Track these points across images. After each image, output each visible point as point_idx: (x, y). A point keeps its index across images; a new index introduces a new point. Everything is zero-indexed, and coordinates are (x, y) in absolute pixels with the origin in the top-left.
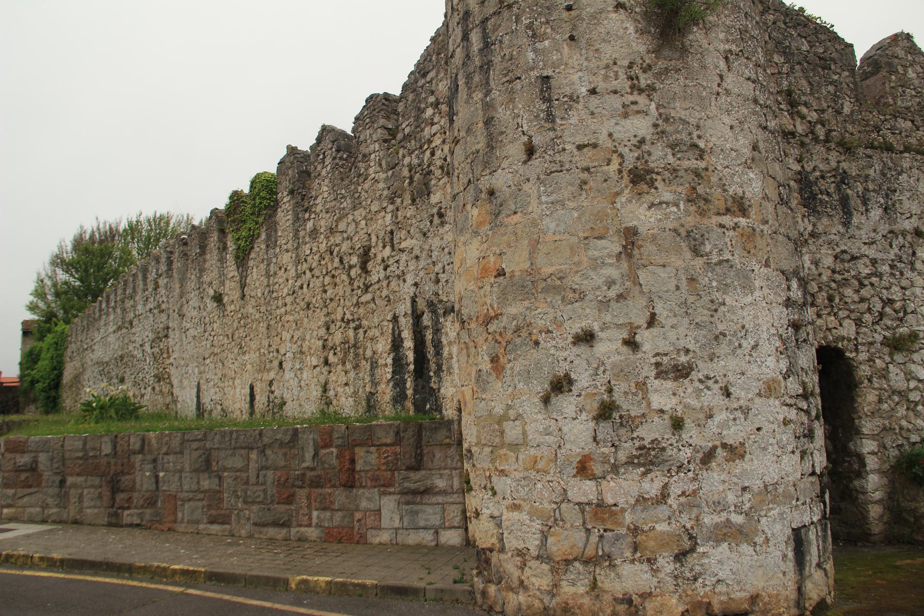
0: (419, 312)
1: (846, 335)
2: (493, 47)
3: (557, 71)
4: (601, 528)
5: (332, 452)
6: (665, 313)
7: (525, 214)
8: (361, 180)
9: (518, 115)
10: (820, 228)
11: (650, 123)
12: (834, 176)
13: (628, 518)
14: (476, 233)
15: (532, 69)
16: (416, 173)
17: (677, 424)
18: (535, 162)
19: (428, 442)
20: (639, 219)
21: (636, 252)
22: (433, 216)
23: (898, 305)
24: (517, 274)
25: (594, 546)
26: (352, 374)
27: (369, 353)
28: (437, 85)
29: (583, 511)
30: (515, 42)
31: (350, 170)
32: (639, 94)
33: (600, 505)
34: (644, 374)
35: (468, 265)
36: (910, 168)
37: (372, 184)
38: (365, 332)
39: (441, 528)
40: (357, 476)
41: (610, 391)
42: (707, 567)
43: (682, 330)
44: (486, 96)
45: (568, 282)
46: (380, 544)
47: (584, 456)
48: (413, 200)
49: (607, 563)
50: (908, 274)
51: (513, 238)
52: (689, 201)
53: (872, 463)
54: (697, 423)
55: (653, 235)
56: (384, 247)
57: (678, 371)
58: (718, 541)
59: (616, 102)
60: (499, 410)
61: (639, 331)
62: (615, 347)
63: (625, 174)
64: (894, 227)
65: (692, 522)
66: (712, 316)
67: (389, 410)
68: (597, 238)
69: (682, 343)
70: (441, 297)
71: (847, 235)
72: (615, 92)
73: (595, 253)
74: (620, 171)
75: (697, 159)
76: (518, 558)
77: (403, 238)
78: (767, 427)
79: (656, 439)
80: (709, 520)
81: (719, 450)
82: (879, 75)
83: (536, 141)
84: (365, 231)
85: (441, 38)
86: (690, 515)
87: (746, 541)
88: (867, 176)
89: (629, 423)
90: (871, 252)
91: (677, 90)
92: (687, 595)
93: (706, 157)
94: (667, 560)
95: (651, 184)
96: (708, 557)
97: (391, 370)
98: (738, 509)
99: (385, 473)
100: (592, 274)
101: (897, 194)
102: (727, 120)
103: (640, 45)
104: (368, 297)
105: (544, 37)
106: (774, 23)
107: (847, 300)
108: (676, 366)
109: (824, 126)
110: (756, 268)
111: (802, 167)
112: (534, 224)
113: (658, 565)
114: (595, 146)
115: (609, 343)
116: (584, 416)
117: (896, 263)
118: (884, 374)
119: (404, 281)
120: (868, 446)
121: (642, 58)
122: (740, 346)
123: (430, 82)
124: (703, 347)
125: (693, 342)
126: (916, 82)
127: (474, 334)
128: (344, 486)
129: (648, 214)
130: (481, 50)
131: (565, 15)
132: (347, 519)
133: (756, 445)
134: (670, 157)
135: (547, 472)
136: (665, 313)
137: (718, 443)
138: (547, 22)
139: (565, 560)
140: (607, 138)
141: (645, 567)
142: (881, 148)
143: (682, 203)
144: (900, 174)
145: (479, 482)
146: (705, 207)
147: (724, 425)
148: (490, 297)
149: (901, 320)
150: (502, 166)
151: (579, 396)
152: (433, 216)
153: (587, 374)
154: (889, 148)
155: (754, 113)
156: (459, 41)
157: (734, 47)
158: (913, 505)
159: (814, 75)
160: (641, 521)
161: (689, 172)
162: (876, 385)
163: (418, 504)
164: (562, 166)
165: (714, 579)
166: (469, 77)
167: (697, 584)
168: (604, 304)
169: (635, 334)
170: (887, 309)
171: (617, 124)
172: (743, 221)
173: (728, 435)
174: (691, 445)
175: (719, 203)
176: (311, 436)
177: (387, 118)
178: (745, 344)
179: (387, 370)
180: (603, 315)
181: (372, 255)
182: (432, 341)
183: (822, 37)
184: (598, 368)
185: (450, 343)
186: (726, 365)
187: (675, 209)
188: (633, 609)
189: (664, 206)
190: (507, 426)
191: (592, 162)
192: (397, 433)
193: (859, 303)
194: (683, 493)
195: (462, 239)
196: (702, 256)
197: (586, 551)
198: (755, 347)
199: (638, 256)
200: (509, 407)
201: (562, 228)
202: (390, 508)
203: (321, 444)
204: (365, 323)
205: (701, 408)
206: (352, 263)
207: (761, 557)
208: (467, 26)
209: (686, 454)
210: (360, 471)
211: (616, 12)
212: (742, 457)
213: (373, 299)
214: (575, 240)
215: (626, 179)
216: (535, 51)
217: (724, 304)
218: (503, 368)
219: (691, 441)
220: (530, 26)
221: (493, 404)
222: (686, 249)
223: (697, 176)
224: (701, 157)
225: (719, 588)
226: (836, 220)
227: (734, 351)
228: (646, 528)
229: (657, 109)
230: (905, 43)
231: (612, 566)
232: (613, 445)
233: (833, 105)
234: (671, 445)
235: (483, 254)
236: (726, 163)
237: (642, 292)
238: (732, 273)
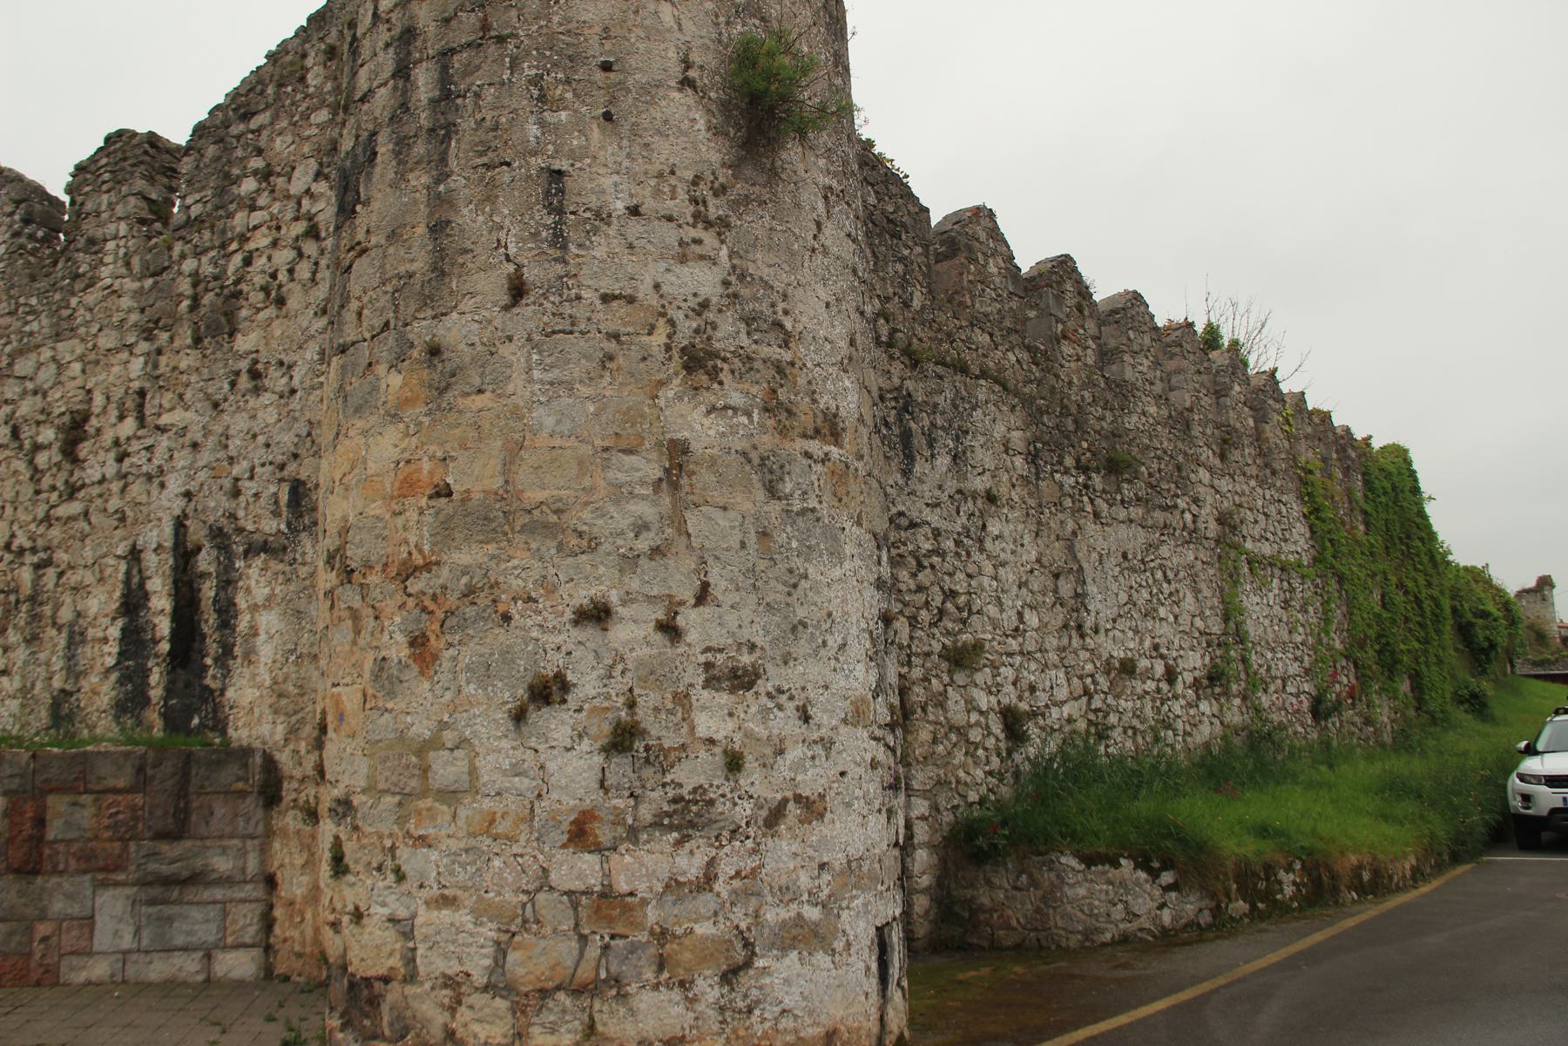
0: (190, 546)
2: (459, 101)
3: (578, 165)
4: (606, 933)
6: (723, 584)
7: (500, 396)
8: (78, 285)
9: (498, 228)
11: (719, 278)
12: (895, 399)
13: (652, 915)
14: (394, 417)
15: (534, 154)
16: (207, 290)
17: (734, 763)
18: (526, 310)
19: (202, 787)
20: (692, 429)
21: (684, 481)
22: (238, 373)
23: (962, 600)
24: (476, 496)
25: (593, 964)
26: (21, 654)
27: (66, 615)
28: (272, 140)
29: (575, 906)
30: (506, 102)
31: (55, 263)
32: (706, 229)
33: (607, 894)
34: (687, 680)
35: (369, 472)
37: (105, 298)
38: (61, 574)
39: (216, 947)
40: (47, 851)
41: (631, 705)
42: (768, 990)
43: (746, 613)
44: (438, 182)
45: (571, 519)
46: (89, 983)
47: (584, 813)
48: (197, 341)
49: (614, 992)
50: (976, 556)
51: (472, 434)
52: (767, 410)
55: (711, 457)
56: (121, 418)
57: (736, 677)
58: (784, 950)
60: (421, 729)
61: (681, 609)
62: (643, 634)
63: (675, 353)
65: (749, 920)
66: (789, 594)
67: (105, 725)
68: (623, 451)
69: (745, 634)
70: (242, 523)
71: (907, 490)
72: (670, 219)
73: (619, 475)
74: (668, 348)
76: (444, 992)
77: (167, 405)
78: (854, 772)
80: (774, 915)
81: (791, 805)
82: (956, 261)
83: (530, 274)
84: (79, 382)
85: (289, 58)
88: (936, 405)
89: (660, 759)
90: (934, 518)
91: (760, 233)
94: (710, 981)
95: (714, 374)
96: (770, 975)
97: (115, 650)
99: (108, 845)
104: (75, 507)
105: (559, 105)
108: (734, 670)
109: (887, 321)
110: (848, 525)
112: (516, 414)
113: (696, 990)
114: (631, 300)
115: (633, 626)
116: (586, 745)
118: (941, 702)
119: (162, 486)
122: (824, 643)
123: (258, 131)
124: (774, 642)
126: (997, 280)
127: (376, 593)
128: (17, 871)
129: (707, 422)
130: (433, 102)
131: (599, 76)
132: (17, 938)
134: (743, 336)
135: (512, 839)
136: (723, 584)
137: (789, 794)
138: (568, 82)
139: (540, 990)
140: (651, 291)
141: (676, 995)
142: (955, 367)
144: (974, 409)
145: (365, 859)
147: (799, 766)
148: (416, 529)
149: (964, 622)
150: (462, 307)
151: (579, 710)
152: (238, 373)
153: (595, 674)
154: (963, 369)
155: (853, 289)
156: (386, 74)
157: (834, 184)
158: (969, 893)
160: (671, 920)
162: (932, 718)
163: (173, 903)
164: (573, 324)
165: (777, 1009)
166: (402, 144)
168: (629, 561)
169: (676, 613)
171: (668, 270)
172: (835, 452)
175: (806, 420)
177: (151, 180)
179: (106, 649)
181: (92, 431)
182: (215, 601)
183: (894, 190)
185: (254, 608)
186: (805, 673)
187: (744, 420)
189: (730, 412)
190: (438, 759)
191: (625, 325)
192: (140, 769)
194: (738, 873)
195: (360, 424)
197: (579, 972)
198: (843, 647)
199: (687, 489)
200: (443, 726)
201: (566, 427)
202: (114, 915)
204: (61, 556)
206: (40, 439)
208: (409, 53)
209: (745, 809)
210: (55, 842)
211: (680, 90)
212: (821, 816)
213: (86, 514)
214: (587, 450)
216: (542, 124)
217: (806, 577)
218: (435, 657)
219: (752, 791)
220: (536, 81)
221: (409, 719)
222: (759, 485)
224: (786, 345)
227: (816, 652)
228: (679, 931)
230: (985, 222)
231: (622, 997)
232: (632, 795)
234: (723, 796)
235: (406, 455)
236: (817, 359)
237: (689, 547)
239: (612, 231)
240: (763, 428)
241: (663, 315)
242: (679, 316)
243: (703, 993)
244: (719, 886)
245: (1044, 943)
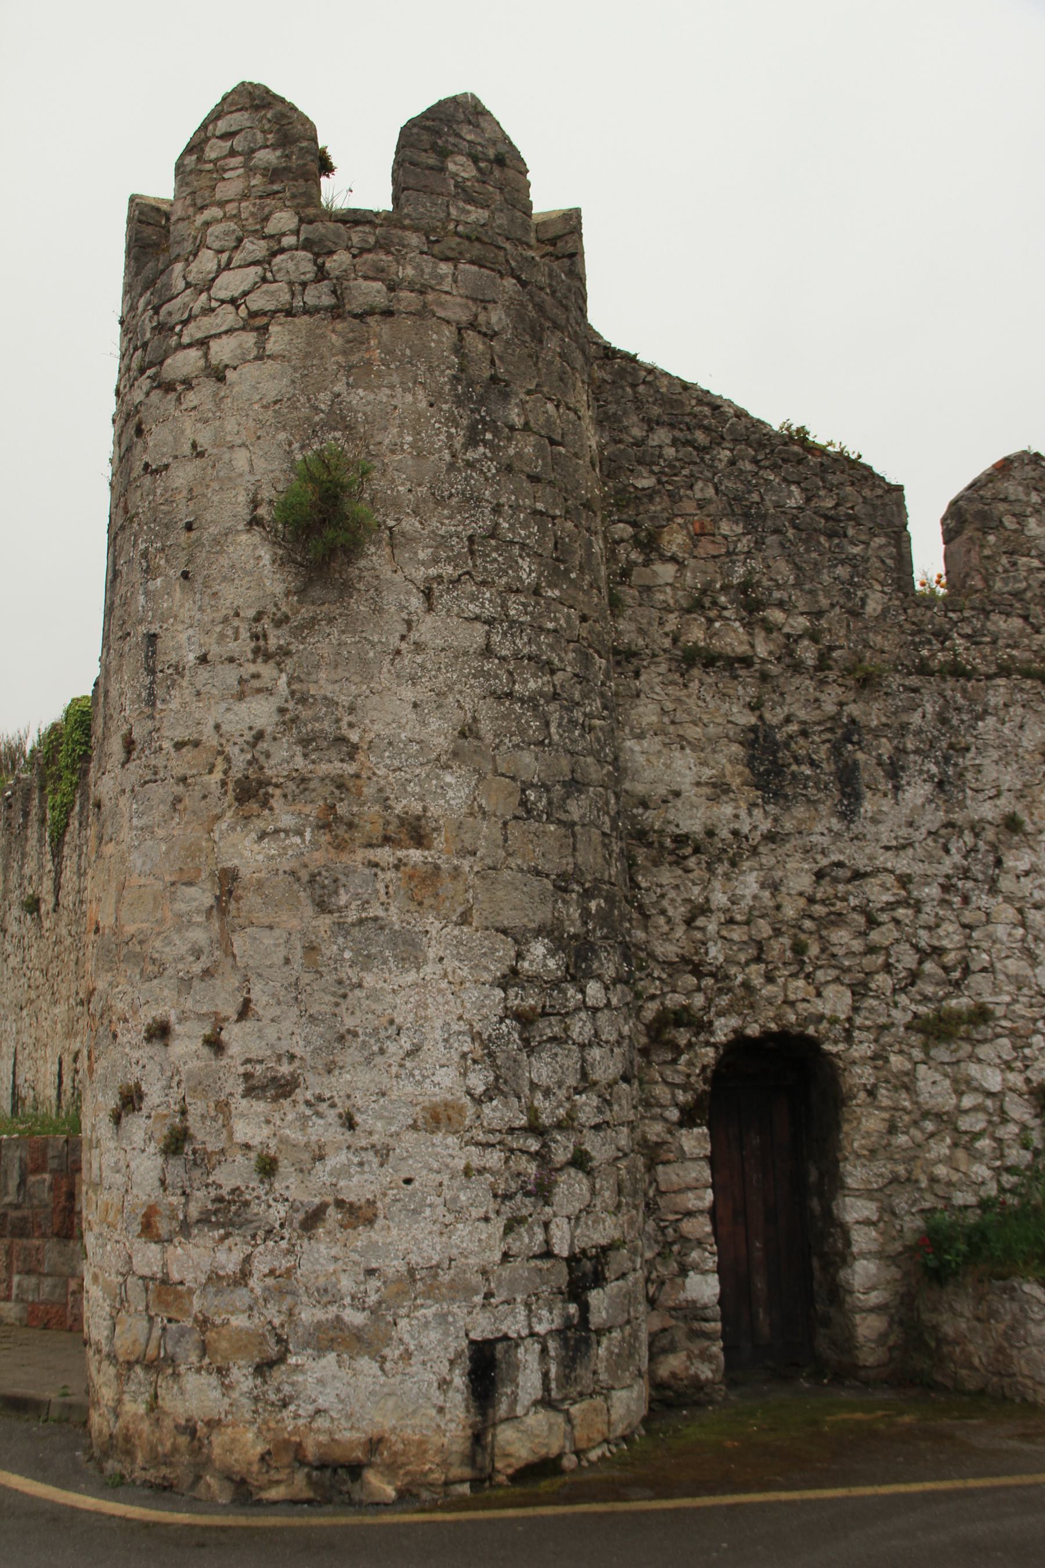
1: (827, 1012)
3: (165, 626)
5: (44, 1180)
6: (265, 999)
10: (789, 825)
12: (831, 730)
13: (197, 1304)
17: (268, 1168)
20: (241, 856)
21: (232, 906)
33: (165, 1281)
34: (228, 1090)
36: (1006, 705)
41: (184, 1112)
43: (287, 1026)
53: (863, 1239)
54: (297, 1166)
55: (259, 881)
58: (321, 1350)
59: (230, 675)
61: (226, 1025)
62: (194, 1048)
63: (231, 786)
64: (958, 817)
65: (282, 1317)
69: (284, 1046)
72: (231, 660)
74: (224, 784)
75: (342, 761)
79: (238, 1188)
80: (309, 1315)
81: (331, 1211)
86: (280, 1306)
87: (369, 1353)
88: (904, 726)
89: (203, 1161)
90: (903, 864)
92: (269, 1429)
93: (361, 756)
94: (245, 1371)
95: (265, 804)
96: (303, 1372)
98: (358, 1302)
100: (176, 938)
101: (969, 755)
102: (408, 693)
103: (276, 584)
106: (732, 462)
107: (835, 950)
108: (274, 1079)
111: (761, 718)
115: (187, 1041)
117: (954, 880)
118: (907, 1083)
120: (855, 1210)
121: (276, 605)
122: (382, 1051)
125: (301, 1043)
128: (57, 1235)
131: (183, 537)
132: (58, 1291)
133: (399, 1205)
136: (265, 999)
137: (330, 1199)
140: (212, 731)
141: (214, 1379)
143: (308, 830)
144: (980, 717)
146: (347, 836)
147: (343, 1171)
149: (957, 984)
159: (808, 551)
160: (213, 1309)
161: (327, 781)
162: (886, 1102)
165: (311, 1408)
167: (285, 1413)
168: (185, 984)
170: (929, 966)
171: (228, 709)
172: (415, 855)
173: (348, 1187)
174: (287, 1200)
176: (18, 1154)
178: (392, 1047)
180: (182, 1000)
184: (173, 1078)
187: (297, 840)
188: (196, 1443)
189: (282, 835)
191: (190, 769)
193: (865, 954)
194: (272, 1272)
196: (331, 912)
198: (413, 1052)
201: (147, 868)
203: (31, 1166)
205: (307, 1145)
207: (392, 1381)
209: (280, 1211)
211: (248, 531)
212: (370, 1222)
215: (230, 796)
217: (360, 986)
219: (286, 1194)
220: (145, 555)
223: (338, 787)
225: (321, 1422)
227: (368, 1060)
228: (218, 1321)
229: (289, 684)
231: (176, 1375)
233: (842, 601)
234: (258, 1198)
236: (397, 763)
237: (235, 967)
238: (382, 938)
239: (185, 683)
240: (315, 845)
241: (221, 753)
242: (233, 751)
243: (238, 1382)
244: (253, 1282)
245: (1008, 1393)
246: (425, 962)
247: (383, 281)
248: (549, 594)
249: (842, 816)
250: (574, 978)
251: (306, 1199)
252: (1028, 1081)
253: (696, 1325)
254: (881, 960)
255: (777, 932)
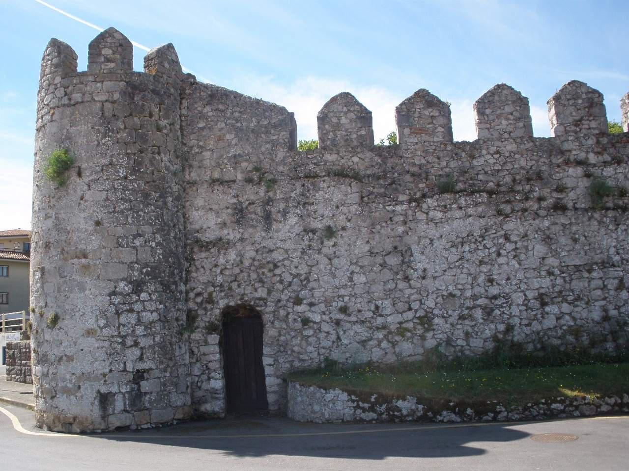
81: (64, 357)
90: (288, 245)
120: (266, 361)
172: (83, 260)
212: (72, 360)
226: (259, 229)
244: (49, 375)
246: (86, 290)
247: (81, 93)
248: (131, 178)
249: (266, 231)
250: (136, 293)
251: (59, 354)
252: (331, 318)
253: (214, 395)
254: (278, 279)
255: (242, 271)
